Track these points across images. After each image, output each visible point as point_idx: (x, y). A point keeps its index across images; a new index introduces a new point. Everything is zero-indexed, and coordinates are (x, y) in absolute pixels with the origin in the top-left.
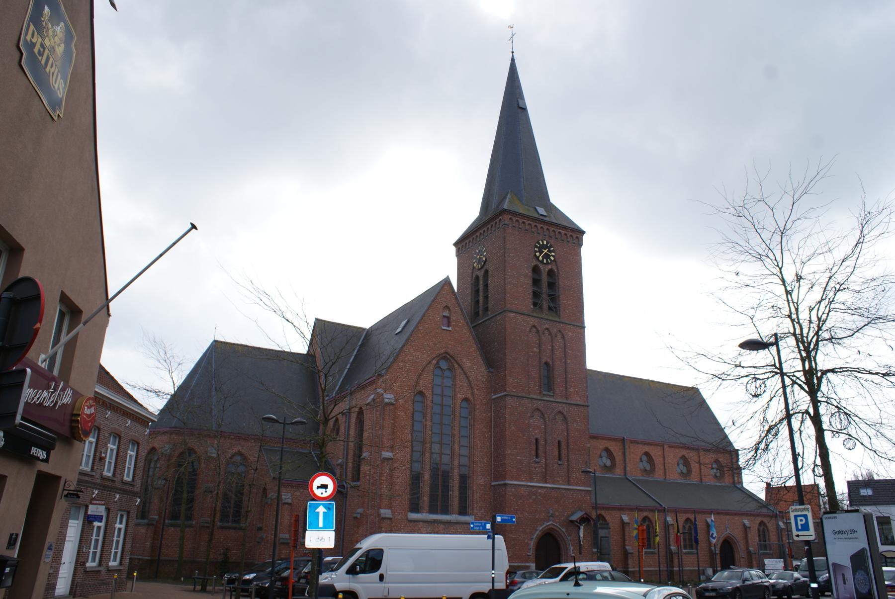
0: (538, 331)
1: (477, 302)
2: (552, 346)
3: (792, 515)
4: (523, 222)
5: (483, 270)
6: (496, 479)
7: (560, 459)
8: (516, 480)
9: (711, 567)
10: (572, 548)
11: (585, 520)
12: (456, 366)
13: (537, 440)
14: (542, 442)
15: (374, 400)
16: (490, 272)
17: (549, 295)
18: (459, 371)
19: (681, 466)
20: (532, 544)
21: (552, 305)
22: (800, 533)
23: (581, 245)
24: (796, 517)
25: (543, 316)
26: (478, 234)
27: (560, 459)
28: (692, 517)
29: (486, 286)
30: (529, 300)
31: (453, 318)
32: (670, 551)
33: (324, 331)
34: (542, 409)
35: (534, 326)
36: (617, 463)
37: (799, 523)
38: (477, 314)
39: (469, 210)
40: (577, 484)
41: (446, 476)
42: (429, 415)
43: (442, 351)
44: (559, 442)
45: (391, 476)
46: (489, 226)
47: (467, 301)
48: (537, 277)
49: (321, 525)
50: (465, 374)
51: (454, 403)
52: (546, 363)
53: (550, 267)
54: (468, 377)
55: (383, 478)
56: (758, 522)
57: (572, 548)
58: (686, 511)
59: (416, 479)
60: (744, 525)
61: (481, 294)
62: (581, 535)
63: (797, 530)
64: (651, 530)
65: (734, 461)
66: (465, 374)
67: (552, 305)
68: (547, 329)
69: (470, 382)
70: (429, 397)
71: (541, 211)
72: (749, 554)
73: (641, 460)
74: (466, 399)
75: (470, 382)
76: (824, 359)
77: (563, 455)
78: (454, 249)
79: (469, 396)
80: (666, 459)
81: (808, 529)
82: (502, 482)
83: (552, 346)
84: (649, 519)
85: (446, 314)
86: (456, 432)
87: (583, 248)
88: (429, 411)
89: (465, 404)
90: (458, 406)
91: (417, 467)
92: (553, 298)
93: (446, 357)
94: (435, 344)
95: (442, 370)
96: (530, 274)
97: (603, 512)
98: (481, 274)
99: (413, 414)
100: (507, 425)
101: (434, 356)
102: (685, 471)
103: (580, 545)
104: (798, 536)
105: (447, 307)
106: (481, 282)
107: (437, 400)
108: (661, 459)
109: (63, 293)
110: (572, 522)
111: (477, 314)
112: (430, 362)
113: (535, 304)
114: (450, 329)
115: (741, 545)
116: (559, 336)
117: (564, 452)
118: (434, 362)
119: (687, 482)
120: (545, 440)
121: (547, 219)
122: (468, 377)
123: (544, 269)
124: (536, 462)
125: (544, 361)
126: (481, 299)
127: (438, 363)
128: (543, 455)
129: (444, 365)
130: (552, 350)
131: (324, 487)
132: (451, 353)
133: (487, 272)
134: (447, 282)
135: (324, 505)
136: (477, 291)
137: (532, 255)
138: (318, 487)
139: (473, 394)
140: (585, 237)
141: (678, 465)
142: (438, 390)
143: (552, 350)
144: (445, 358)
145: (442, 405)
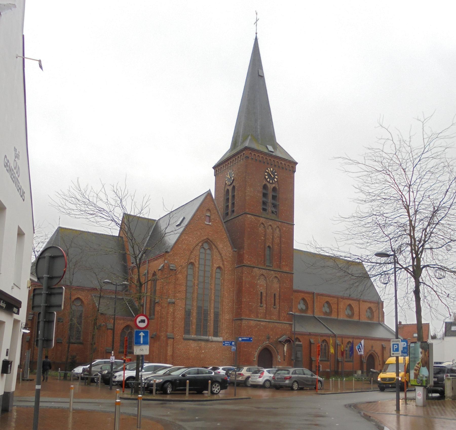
0: (264, 227)
1: (227, 206)
2: (273, 236)
3: (392, 343)
4: (258, 156)
5: (232, 186)
9: (360, 369)
11: (288, 341)
12: (214, 247)
13: (261, 293)
14: (264, 295)
15: (163, 267)
16: (236, 188)
17: (273, 204)
18: (215, 250)
19: (348, 310)
20: (256, 354)
22: (394, 353)
24: (393, 345)
25: (268, 217)
26: (229, 162)
27: (275, 305)
28: (351, 340)
29: (233, 196)
31: (212, 217)
32: (338, 360)
33: (129, 222)
34: (265, 275)
35: (263, 224)
36: (309, 307)
37: (395, 348)
38: (227, 214)
39: (222, 146)
41: (206, 313)
42: (196, 277)
43: (205, 238)
46: (237, 157)
47: (221, 205)
48: (265, 192)
49: (142, 342)
50: (219, 252)
51: (212, 270)
52: (269, 247)
53: (274, 185)
54: (220, 254)
55: (169, 314)
58: (348, 337)
59: (188, 314)
61: (230, 201)
62: (285, 349)
63: (393, 351)
64: (327, 347)
65: (380, 308)
66: (219, 252)
68: (270, 225)
69: (222, 257)
70: (197, 265)
71: (270, 148)
74: (219, 268)
75: (222, 257)
76: (426, 258)
78: (213, 171)
79: (221, 266)
80: (339, 306)
81: (398, 351)
83: (273, 236)
84: (326, 341)
85: (208, 214)
86: (213, 287)
88: (197, 274)
89: (218, 270)
90: (214, 272)
91: (189, 307)
93: (207, 241)
94: (201, 233)
95: (205, 249)
97: (299, 337)
98: (230, 188)
99: (187, 276)
100: (244, 284)
101: (200, 240)
104: (393, 354)
105: (209, 210)
106: (230, 194)
107: (202, 268)
108: (336, 306)
109: (19, 229)
110: (280, 342)
111: (227, 214)
112: (197, 245)
114: (210, 224)
116: (278, 230)
118: (200, 244)
120: (266, 294)
121: (274, 154)
122: (220, 254)
123: (271, 187)
124: (260, 306)
125: (267, 245)
127: (202, 245)
128: (265, 302)
129: (206, 246)
130: (273, 239)
131: (143, 321)
132: (211, 239)
133: (234, 187)
134: (209, 194)
135: (143, 332)
136: (228, 199)
138: (139, 322)
139: (223, 264)
141: (346, 309)
142: (202, 262)
143: (273, 239)
144: (206, 242)
145: (205, 271)
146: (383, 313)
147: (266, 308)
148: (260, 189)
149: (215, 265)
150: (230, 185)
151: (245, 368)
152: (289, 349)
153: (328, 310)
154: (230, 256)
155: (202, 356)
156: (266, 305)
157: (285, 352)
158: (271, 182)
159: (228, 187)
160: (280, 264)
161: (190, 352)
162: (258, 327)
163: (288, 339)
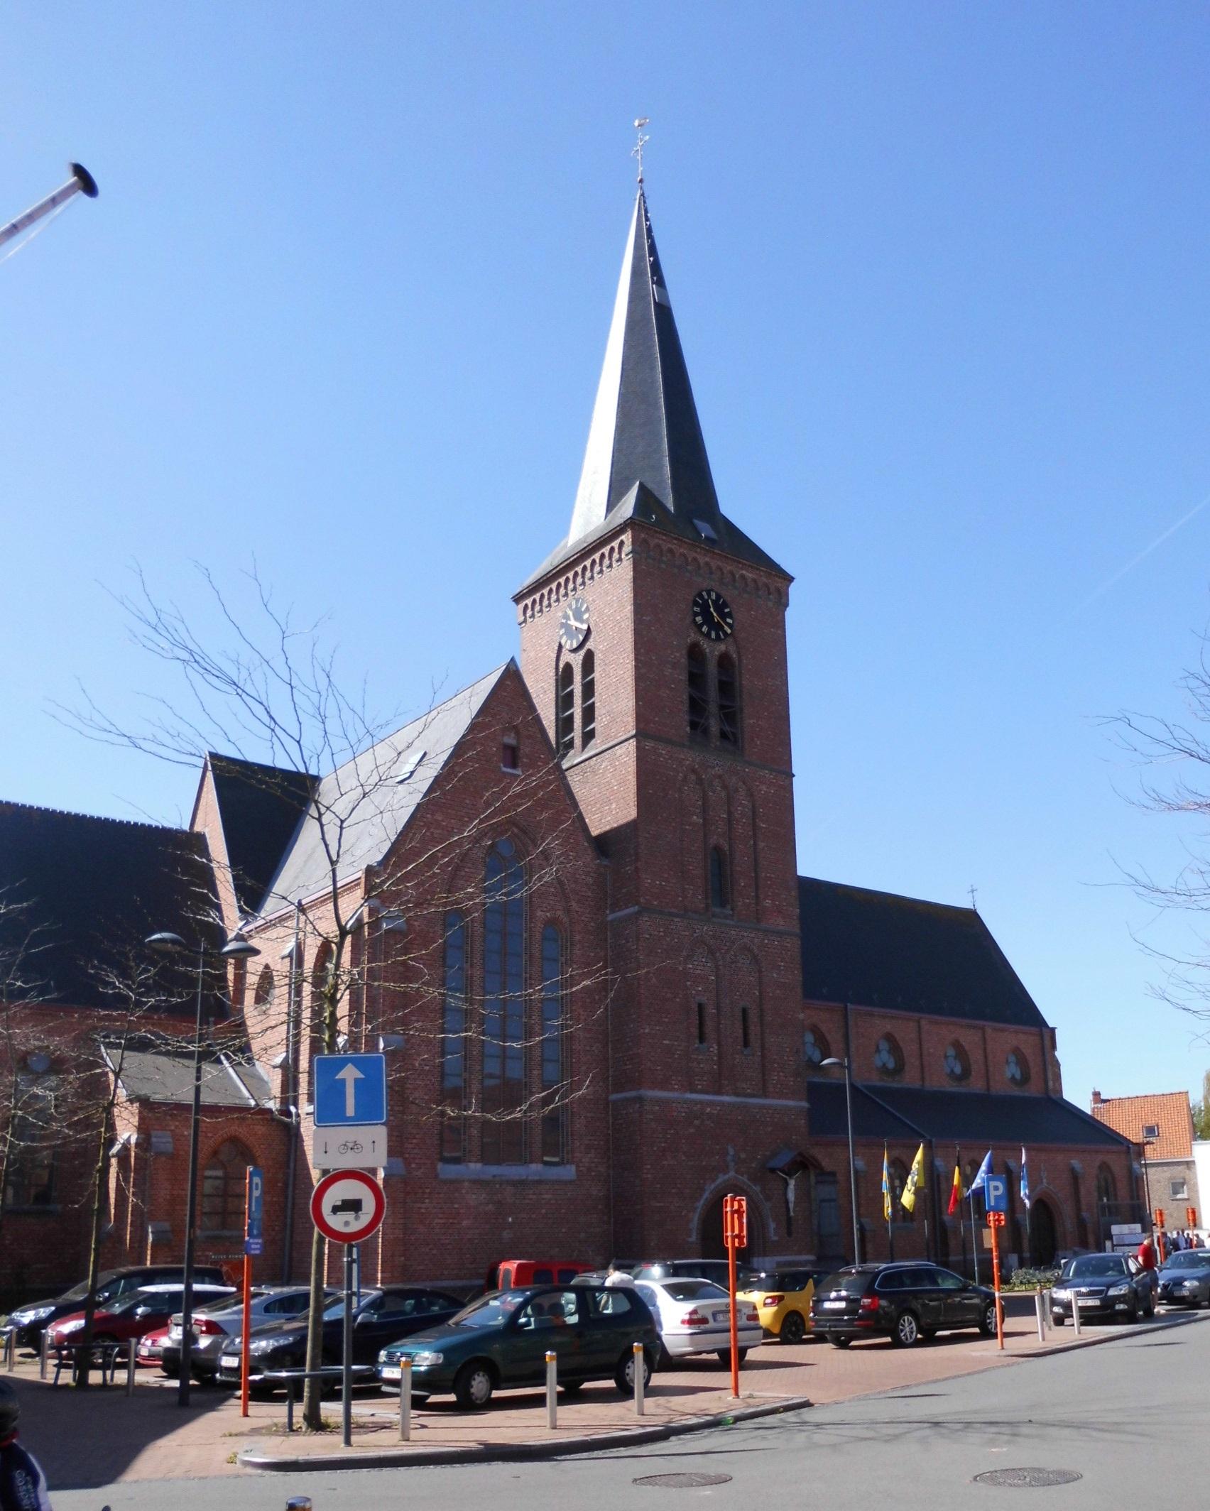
2: (730, 813)
5: (582, 653)
6: (619, 1087)
7: (746, 1044)
8: (662, 1089)
10: (772, 1226)
14: (711, 1010)
19: (951, 1060)
21: (727, 728)
23: (787, 605)
29: (589, 689)
30: (683, 718)
35: (694, 771)
40: (781, 1095)
44: (745, 1011)
45: (292, 1237)
49: (350, 1111)
52: (717, 849)
53: (722, 647)
56: (1097, 1164)
57: (772, 1226)
60: (1073, 1170)
62: (791, 1196)
67: (727, 728)
68: (720, 777)
72: (1081, 1224)
73: (878, 1050)
77: (752, 1037)
82: (633, 1094)
83: (730, 813)
85: (510, 740)
87: (789, 613)
92: (730, 715)
96: (684, 661)
98: (577, 661)
102: (958, 1070)
103: (789, 1219)
110: (773, 1170)
113: (694, 725)
115: (1067, 1209)
117: (754, 1029)
119: (962, 1090)
120: (718, 1008)
126: (577, 711)
137: (688, 620)
138: (336, 1209)
139: (568, 911)
140: (793, 589)
146: (1057, 1065)
147: (720, 1055)
148: (681, 657)
149: (539, 913)
150: (574, 651)
151: (656, 1270)
152: (804, 1194)
153: (891, 1065)
154: (591, 880)
155: (506, 1234)
156: (719, 1045)
157: (791, 1206)
158: (713, 635)
159: (567, 657)
160: (757, 904)
161: (465, 1223)
162: (697, 1122)
163: (799, 1159)
